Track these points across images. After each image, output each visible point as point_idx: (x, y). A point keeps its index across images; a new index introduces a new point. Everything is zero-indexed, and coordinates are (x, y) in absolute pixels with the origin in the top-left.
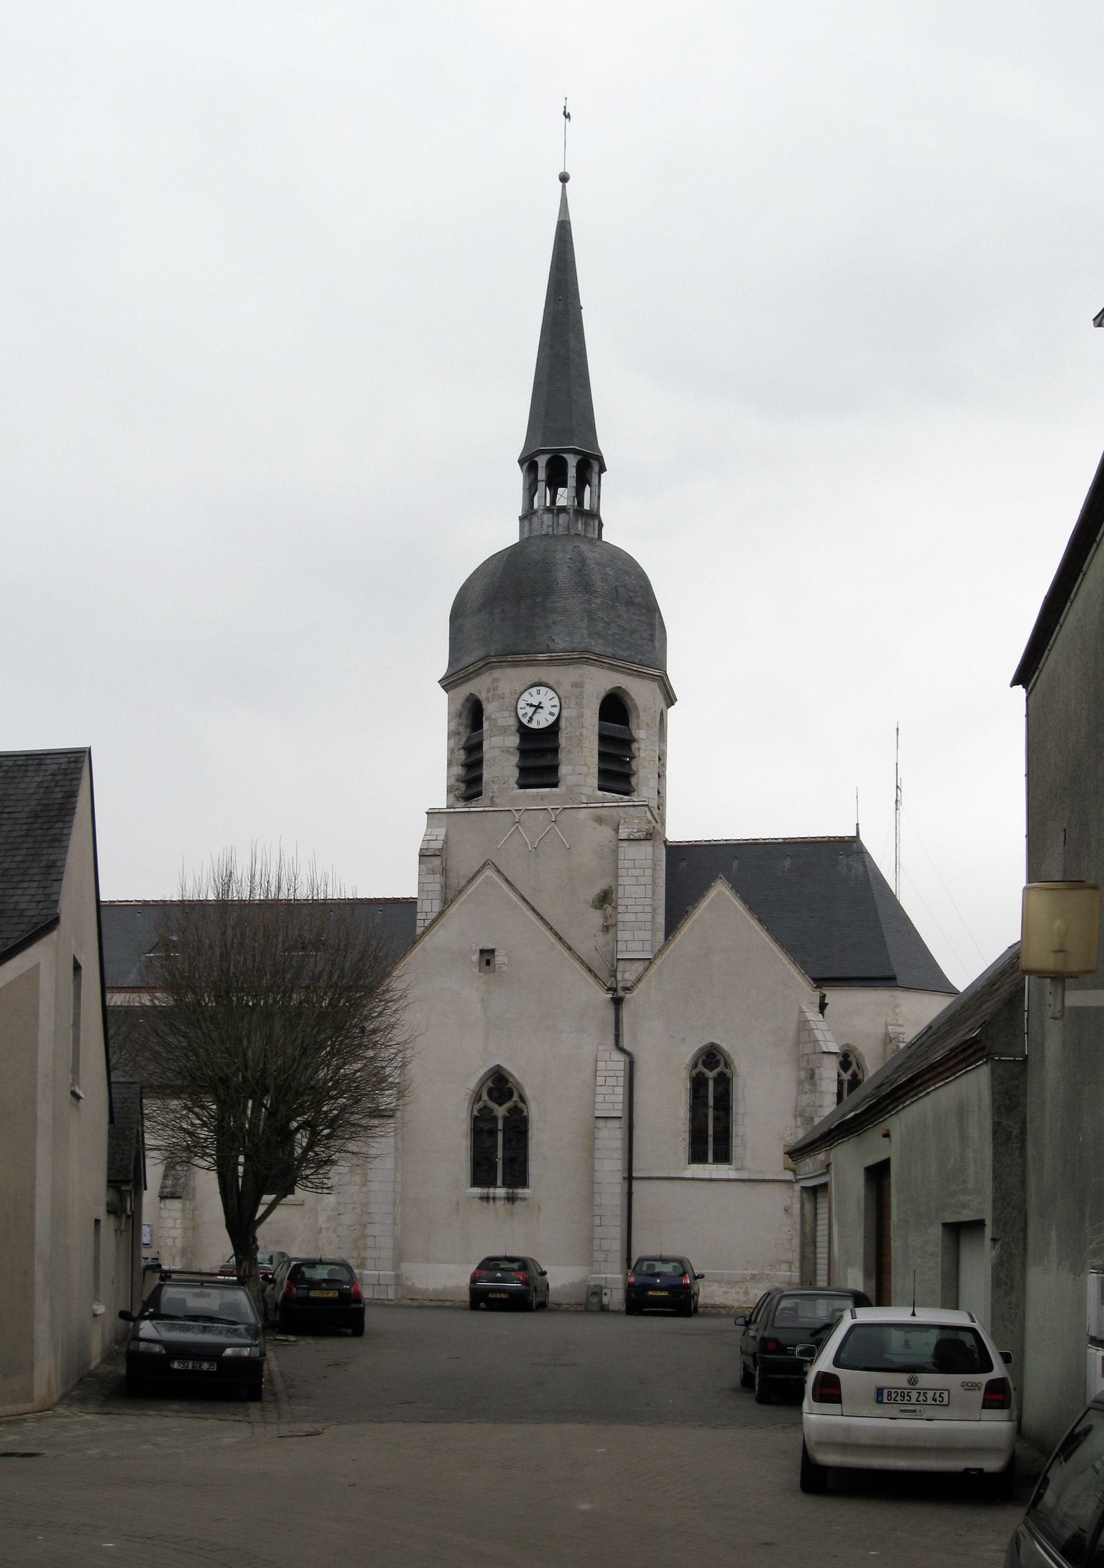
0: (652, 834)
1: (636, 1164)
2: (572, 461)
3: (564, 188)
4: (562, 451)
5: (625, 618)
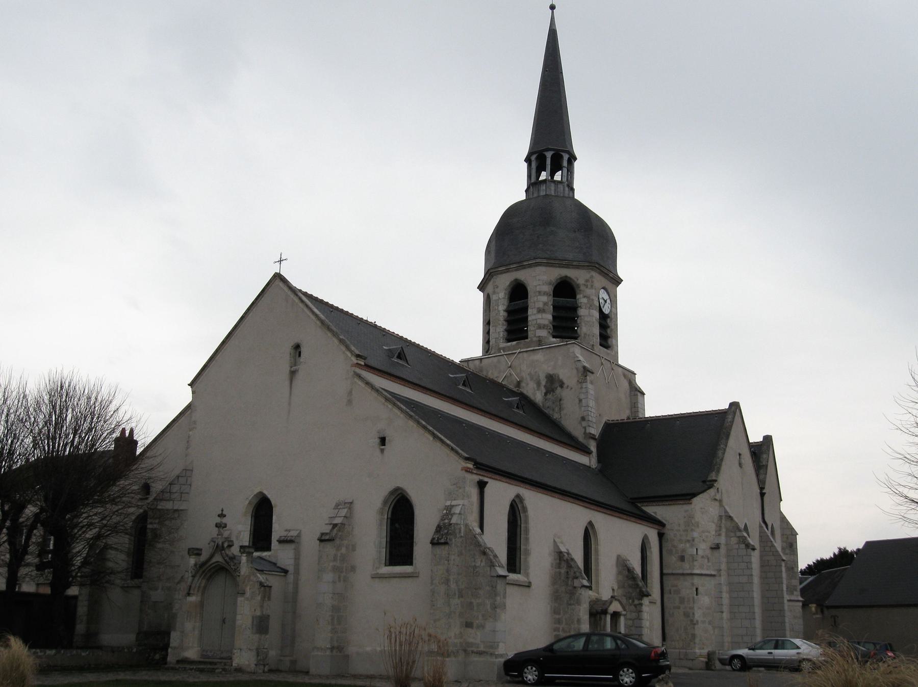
0: (481, 359)
1: (512, 587)
2: (549, 155)
3: (553, 13)
4: (551, 151)
5: (594, 243)
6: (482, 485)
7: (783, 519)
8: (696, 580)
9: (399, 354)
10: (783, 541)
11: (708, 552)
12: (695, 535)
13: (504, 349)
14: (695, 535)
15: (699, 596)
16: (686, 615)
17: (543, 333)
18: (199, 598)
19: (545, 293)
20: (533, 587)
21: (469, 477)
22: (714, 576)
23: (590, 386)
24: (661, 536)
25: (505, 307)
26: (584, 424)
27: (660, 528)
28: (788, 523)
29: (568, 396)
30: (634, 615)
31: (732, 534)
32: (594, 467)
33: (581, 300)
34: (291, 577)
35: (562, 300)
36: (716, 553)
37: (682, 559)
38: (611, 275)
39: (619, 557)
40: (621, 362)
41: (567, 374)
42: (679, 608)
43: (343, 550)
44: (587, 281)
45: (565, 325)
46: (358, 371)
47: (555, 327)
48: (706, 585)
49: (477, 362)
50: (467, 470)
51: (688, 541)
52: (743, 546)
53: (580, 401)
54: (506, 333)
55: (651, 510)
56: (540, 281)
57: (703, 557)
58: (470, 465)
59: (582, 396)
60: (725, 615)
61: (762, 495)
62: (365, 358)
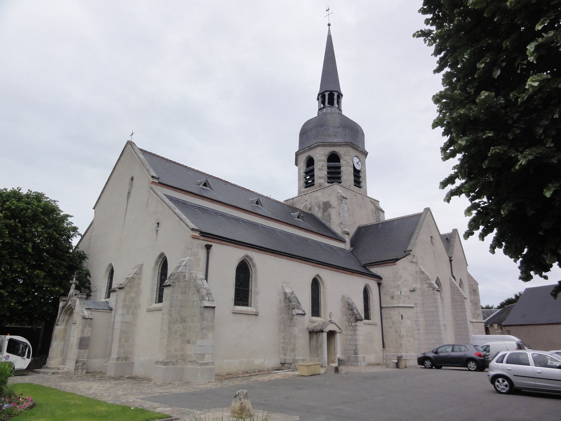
2: (327, 94)
5: (353, 135)
6: (208, 247)
7: (469, 276)
8: (402, 311)
9: (257, 202)
10: (470, 289)
11: (409, 293)
12: (399, 283)
13: (303, 192)
14: (399, 283)
15: (403, 320)
16: (396, 332)
17: (322, 181)
18: (63, 327)
19: (322, 161)
20: (260, 314)
21: (197, 241)
22: (413, 307)
23: (345, 206)
24: (379, 284)
25: (304, 171)
26: (342, 226)
27: (379, 280)
28: (472, 278)
29: (333, 212)
30: (352, 333)
31: (425, 282)
32: (348, 249)
33: (342, 162)
34: (113, 312)
35: (332, 164)
36: (414, 294)
37: (392, 298)
38: (360, 149)
39: (343, 297)
40: (369, 195)
41: (334, 201)
42: (392, 327)
43: (133, 294)
44: (345, 152)
45: (334, 176)
46: (154, 186)
47: (329, 178)
48: (407, 313)
49: (291, 201)
50: (194, 237)
51: (395, 287)
52: (431, 289)
53: (340, 214)
54: (304, 184)
55: (375, 270)
56: (320, 156)
57: (405, 296)
58: (197, 234)
59: (340, 211)
60: (421, 332)
61: (451, 261)
62: (158, 179)
